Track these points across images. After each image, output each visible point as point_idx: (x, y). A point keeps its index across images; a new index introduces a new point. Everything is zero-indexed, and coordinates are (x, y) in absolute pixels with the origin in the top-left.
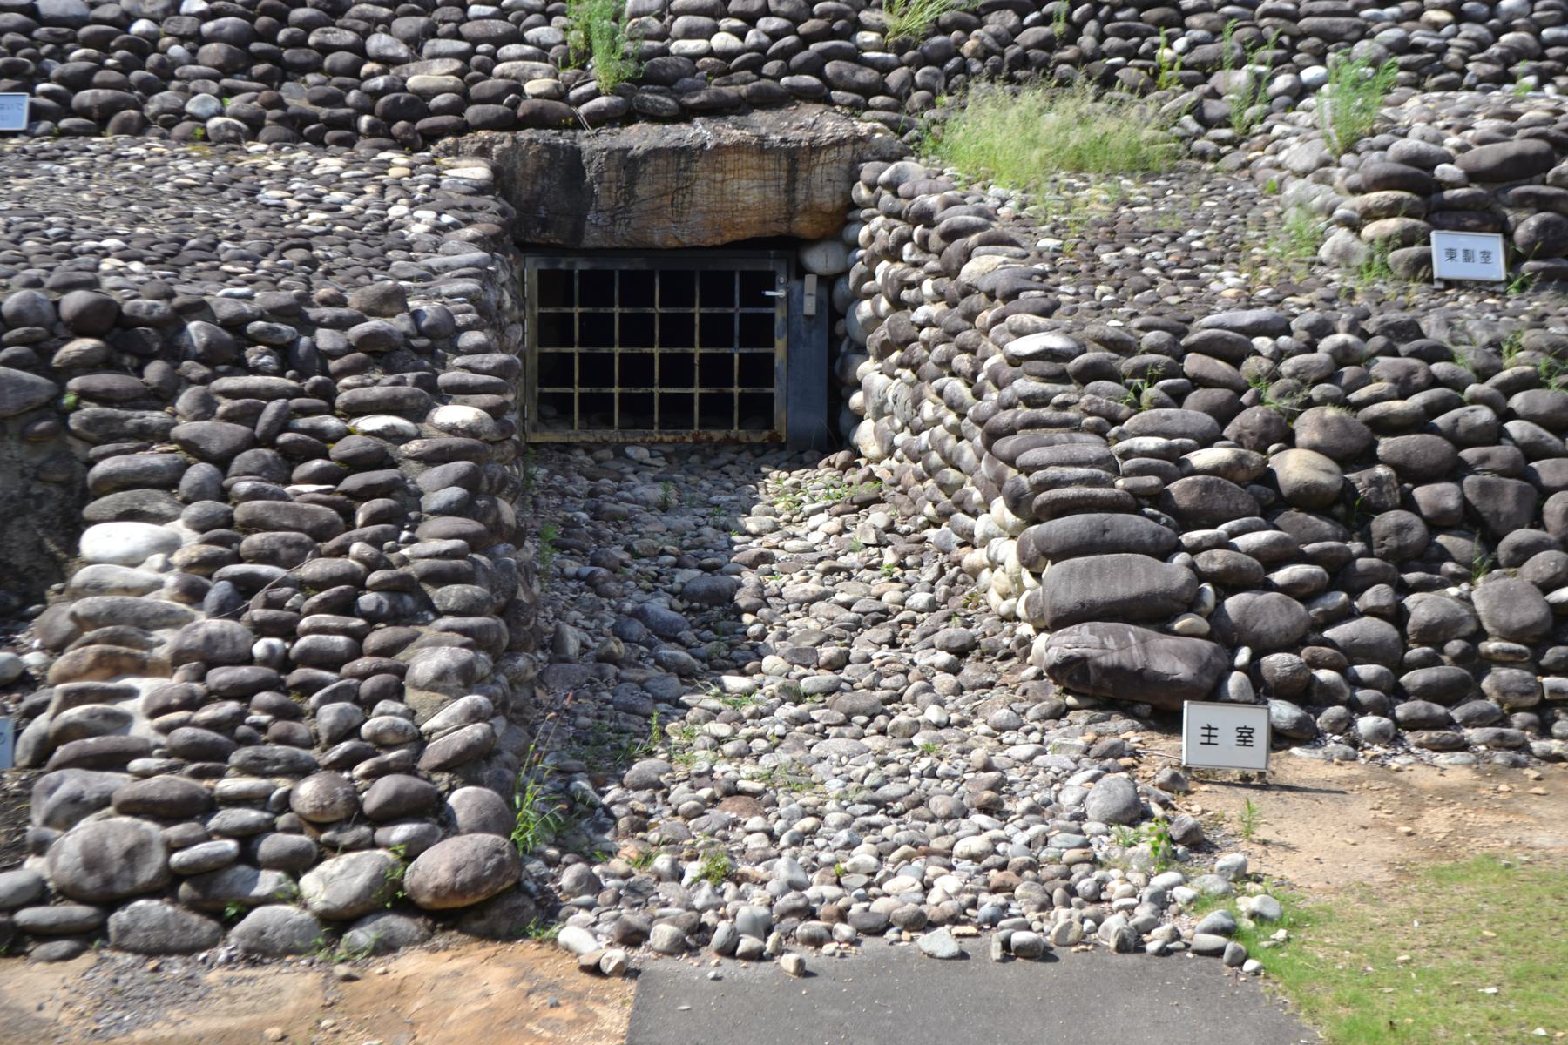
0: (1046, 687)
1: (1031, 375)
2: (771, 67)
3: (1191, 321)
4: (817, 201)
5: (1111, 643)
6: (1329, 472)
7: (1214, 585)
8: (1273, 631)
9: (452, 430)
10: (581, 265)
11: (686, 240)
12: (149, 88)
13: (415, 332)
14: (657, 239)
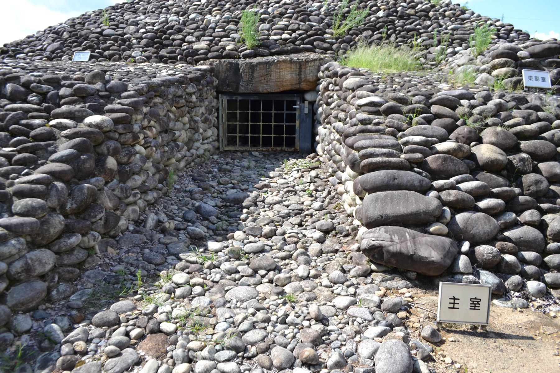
0: (361, 257)
1: (364, 111)
2: (298, 43)
3: (433, 94)
4: (308, 78)
5: (396, 238)
6: (502, 154)
7: (450, 208)
8: (481, 233)
9: (90, 125)
10: (239, 98)
11: (269, 90)
12: (124, 50)
13: (104, 89)
14: (260, 90)
